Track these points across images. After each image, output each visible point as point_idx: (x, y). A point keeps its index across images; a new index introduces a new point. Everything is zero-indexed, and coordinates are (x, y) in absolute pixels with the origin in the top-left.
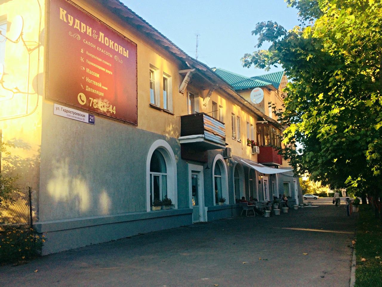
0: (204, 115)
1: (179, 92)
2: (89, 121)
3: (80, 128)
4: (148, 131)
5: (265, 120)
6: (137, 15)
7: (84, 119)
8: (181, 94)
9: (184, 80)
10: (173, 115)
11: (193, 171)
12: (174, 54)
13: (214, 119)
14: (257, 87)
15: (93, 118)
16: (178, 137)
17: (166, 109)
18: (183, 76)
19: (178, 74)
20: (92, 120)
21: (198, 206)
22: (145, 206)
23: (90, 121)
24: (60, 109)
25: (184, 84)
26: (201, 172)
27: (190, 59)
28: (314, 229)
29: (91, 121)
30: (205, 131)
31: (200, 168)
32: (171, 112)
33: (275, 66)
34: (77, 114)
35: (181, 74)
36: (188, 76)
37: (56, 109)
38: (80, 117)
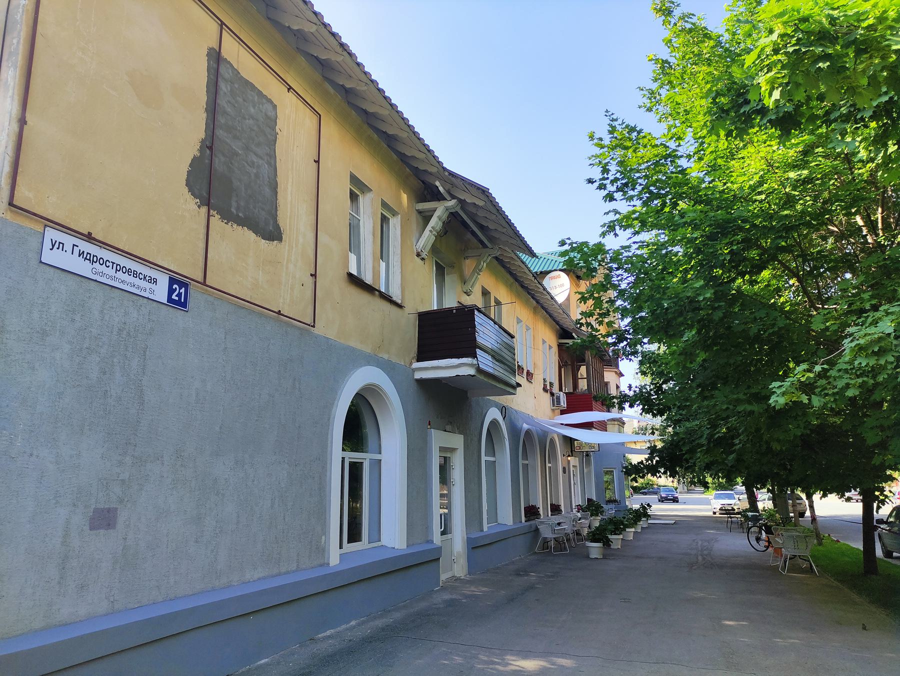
0: (476, 312)
1: (415, 253)
2: (170, 299)
3: (135, 315)
4: (342, 341)
5: (576, 337)
6: (326, 26)
7: (152, 292)
8: (418, 260)
9: (429, 227)
10: (400, 306)
11: (442, 449)
12: (404, 159)
13: (495, 323)
14: (556, 270)
15: (183, 290)
16: (411, 364)
17: (384, 291)
18: (425, 217)
19: (415, 211)
20: (179, 295)
21: (449, 536)
22: (322, 551)
23: (174, 297)
24: (68, 247)
25: (427, 238)
26: (458, 451)
27: (447, 174)
28: (487, 490)
29: (177, 298)
30: (478, 351)
31: (457, 441)
32: (397, 298)
33: (620, 213)
34: (129, 271)
35: (420, 212)
36: (438, 217)
37: (53, 246)
38: (137, 281)
